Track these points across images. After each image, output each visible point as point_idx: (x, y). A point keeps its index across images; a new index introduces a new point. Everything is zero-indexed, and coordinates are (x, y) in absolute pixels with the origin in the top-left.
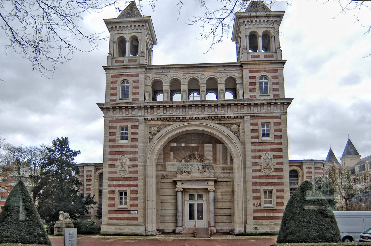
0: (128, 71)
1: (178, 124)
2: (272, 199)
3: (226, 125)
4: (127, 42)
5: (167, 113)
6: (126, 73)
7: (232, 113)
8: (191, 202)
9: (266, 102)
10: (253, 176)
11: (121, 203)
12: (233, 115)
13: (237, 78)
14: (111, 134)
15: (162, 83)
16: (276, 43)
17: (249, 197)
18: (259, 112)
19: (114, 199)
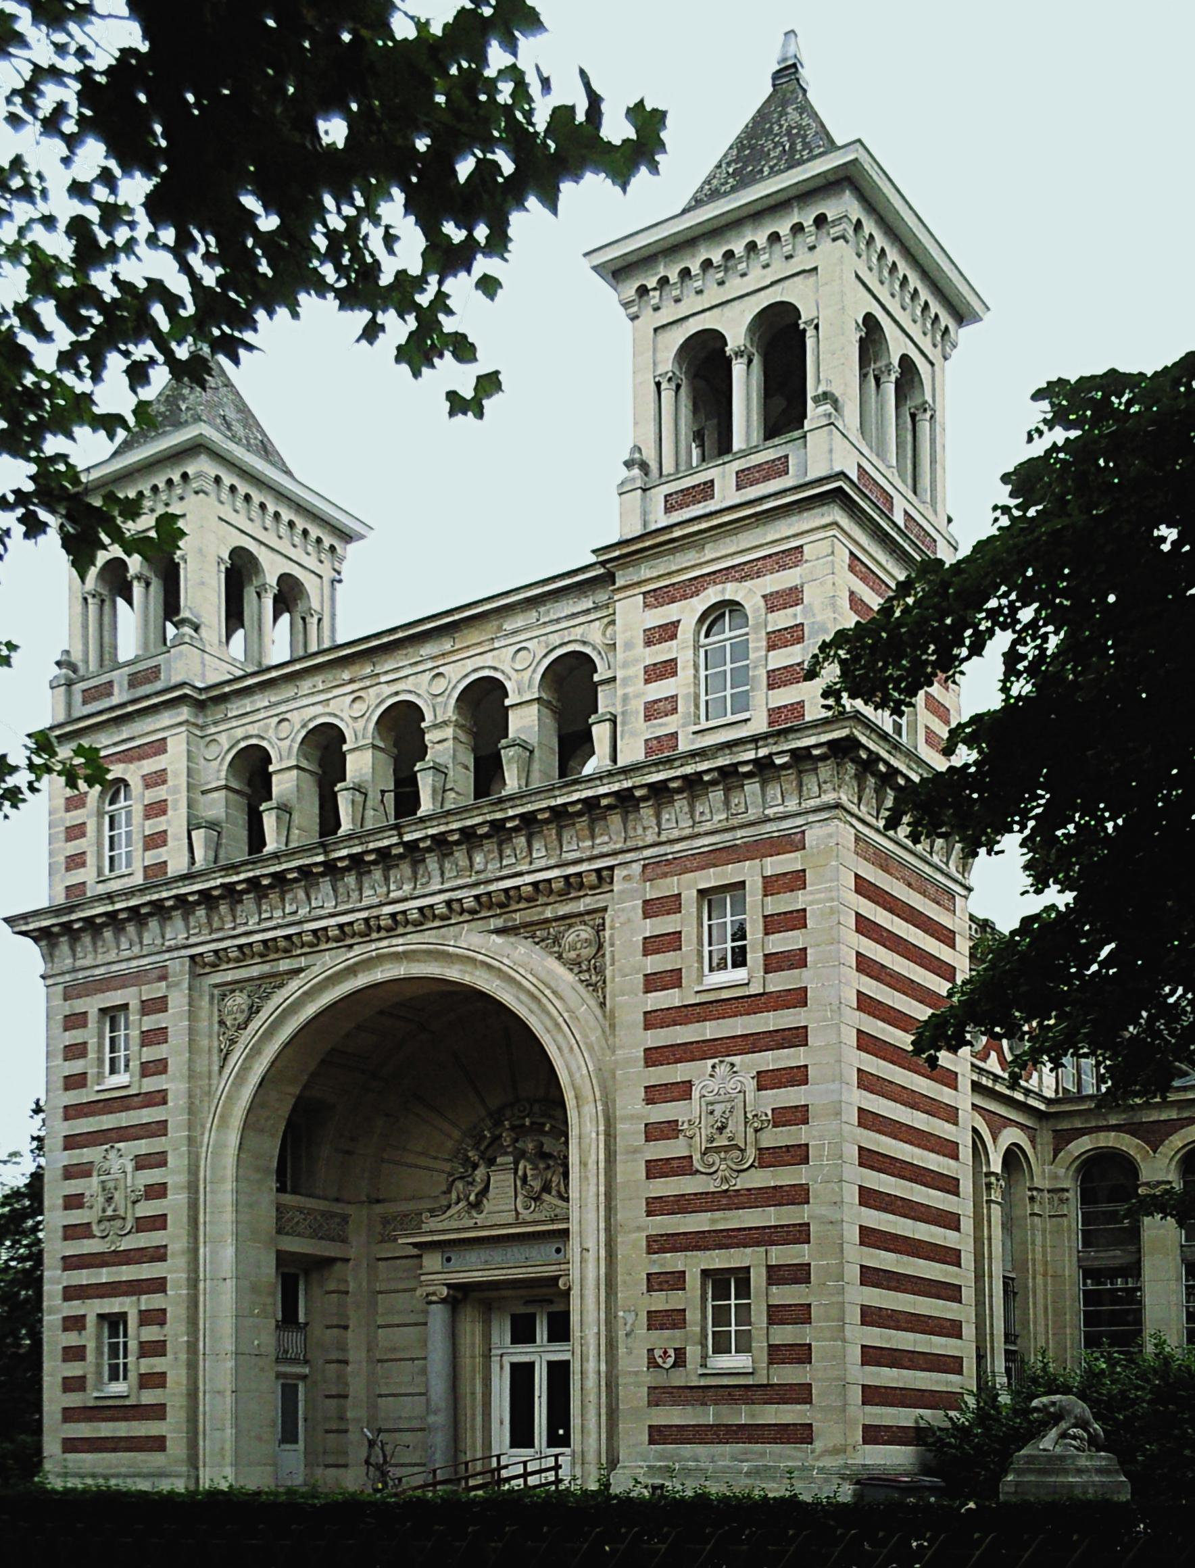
1: (330, 961)
2: (106, 1341)
3: (538, 933)
4: (135, 583)
6: (115, 744)
8: (522, 1353)
9: (705, 766)
10: (650, 1201)
13: (600, 653)
17: (630, 1319)
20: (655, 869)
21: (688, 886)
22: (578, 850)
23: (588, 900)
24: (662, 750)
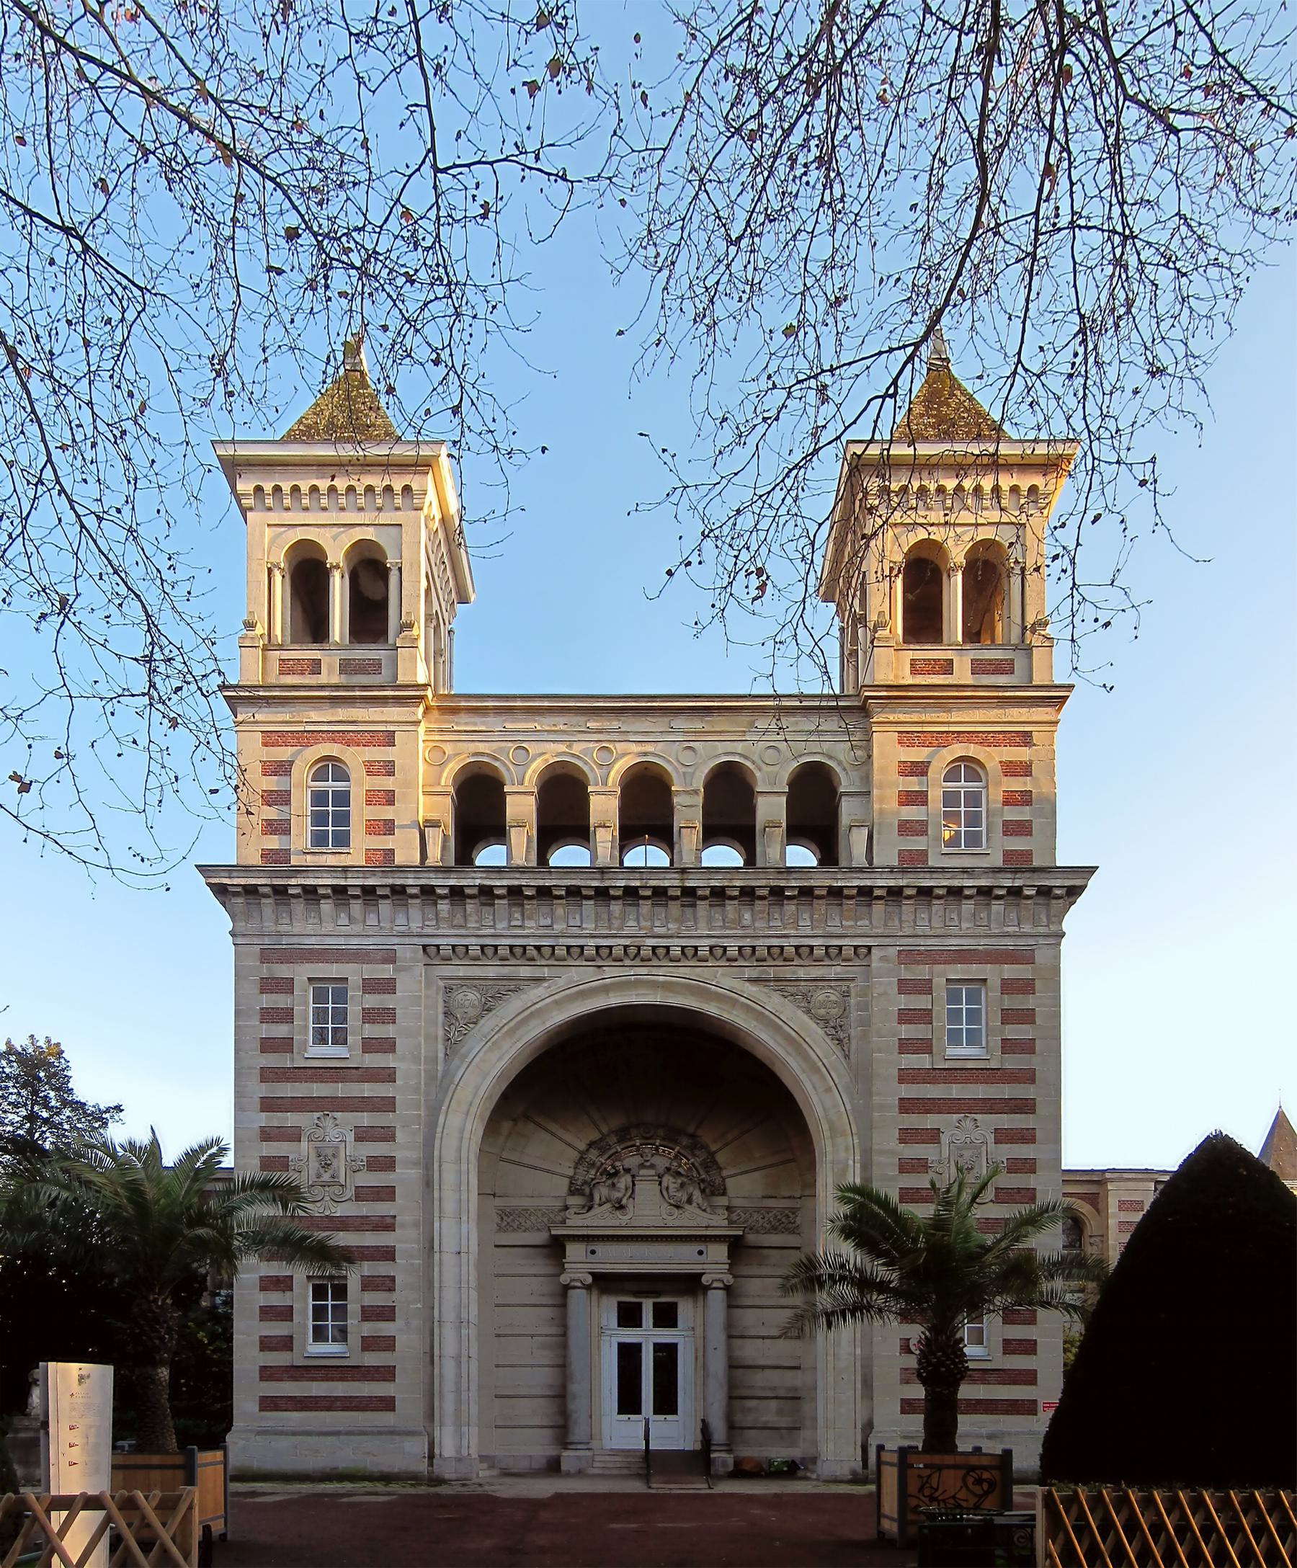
0: (342, 713)
1: (577, 974)
5: (528, 923)
7: (820, 932)
8: (630, 1335)
11: (319, 1334)
12: (592, 942)
13: (844, 769)
14: (269, 1015)
15: (502, 785)
16: (1028, 600)
18: (939, 932)
19: (285, 1314)
20: (908, 956)
21: (941, 975)
22: (845, 927)
23: (839, 969)
24: (913, 862)
